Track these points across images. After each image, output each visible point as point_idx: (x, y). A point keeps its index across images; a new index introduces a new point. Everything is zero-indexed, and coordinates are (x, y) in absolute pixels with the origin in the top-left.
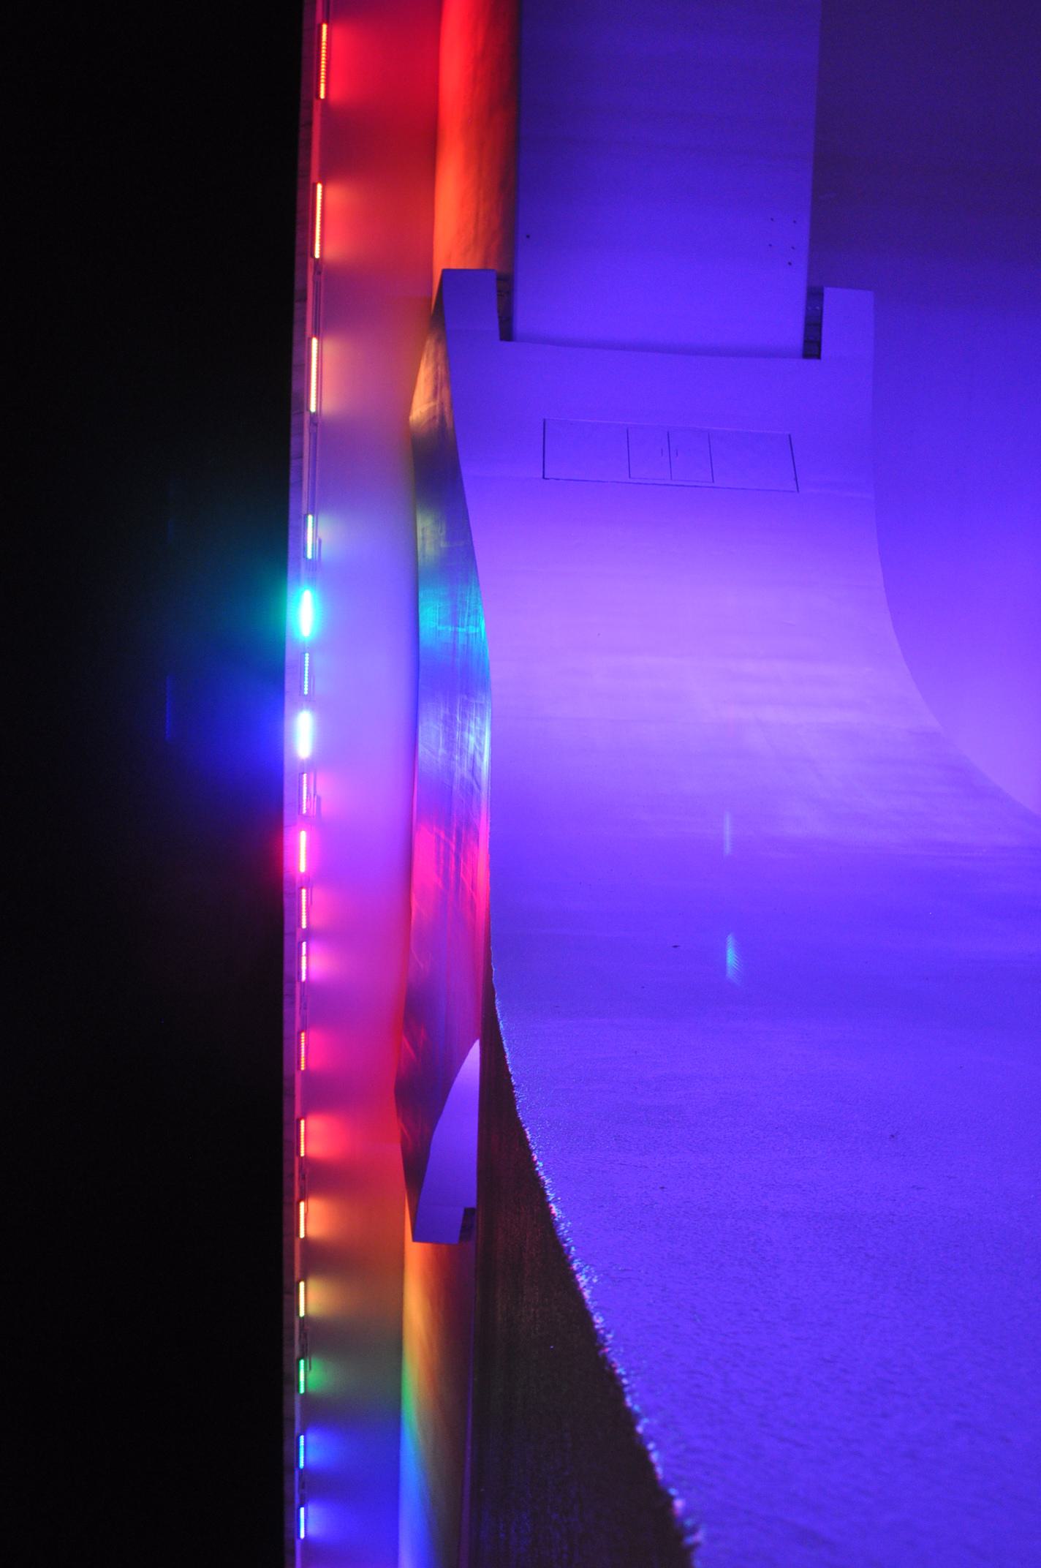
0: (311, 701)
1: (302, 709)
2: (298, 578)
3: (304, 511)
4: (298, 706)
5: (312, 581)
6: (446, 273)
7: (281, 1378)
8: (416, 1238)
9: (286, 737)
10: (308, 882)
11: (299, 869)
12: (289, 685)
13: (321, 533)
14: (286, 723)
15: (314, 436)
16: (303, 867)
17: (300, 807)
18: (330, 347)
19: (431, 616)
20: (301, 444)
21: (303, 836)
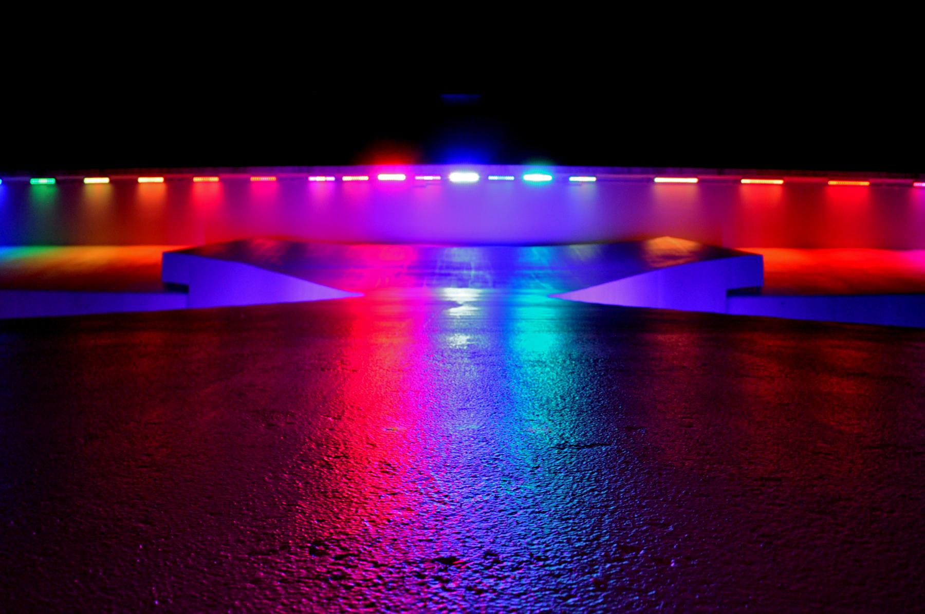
0: (484, 180)
1: (480, 175)
2: (558, 172)
3: (598, 175)
4: (407, 173)
5: (556, 181)
6: (759, 258)
7: (264, 163)
8: (166, 255)
9: (461, 166)
10: (339, 181)
11: (380, 173)
12: (495, 168)
13: (585, 186)
14: (471, 166)
15: (641, 181)
16: (382, 177)
17: (419, 175)
18: (693, 191)
19: (537, 255)
20: (636, 173)
21: (400, 177)
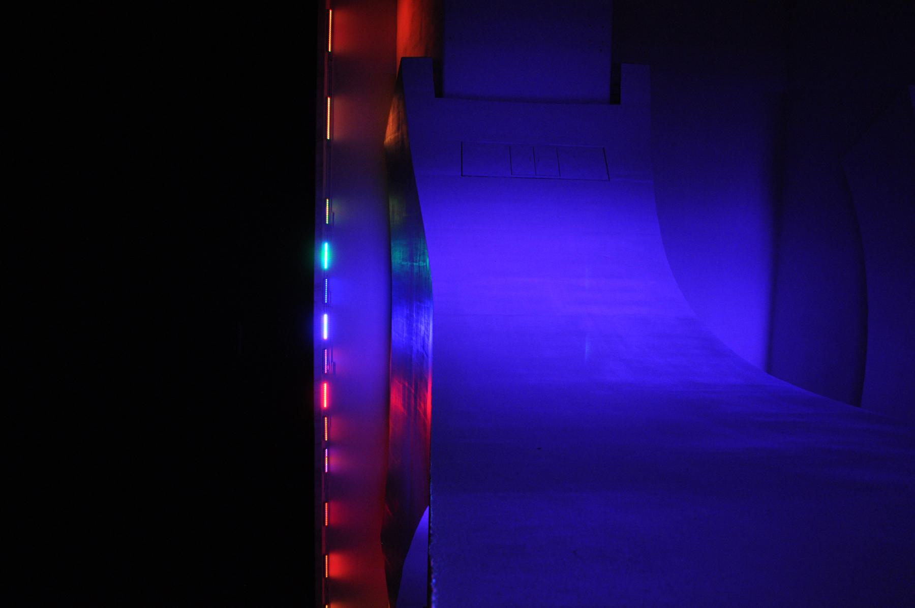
0: (327, 377)
6: (402, 58)
12: (316, 297)
13: (334, 209)
19: (398, 257)
